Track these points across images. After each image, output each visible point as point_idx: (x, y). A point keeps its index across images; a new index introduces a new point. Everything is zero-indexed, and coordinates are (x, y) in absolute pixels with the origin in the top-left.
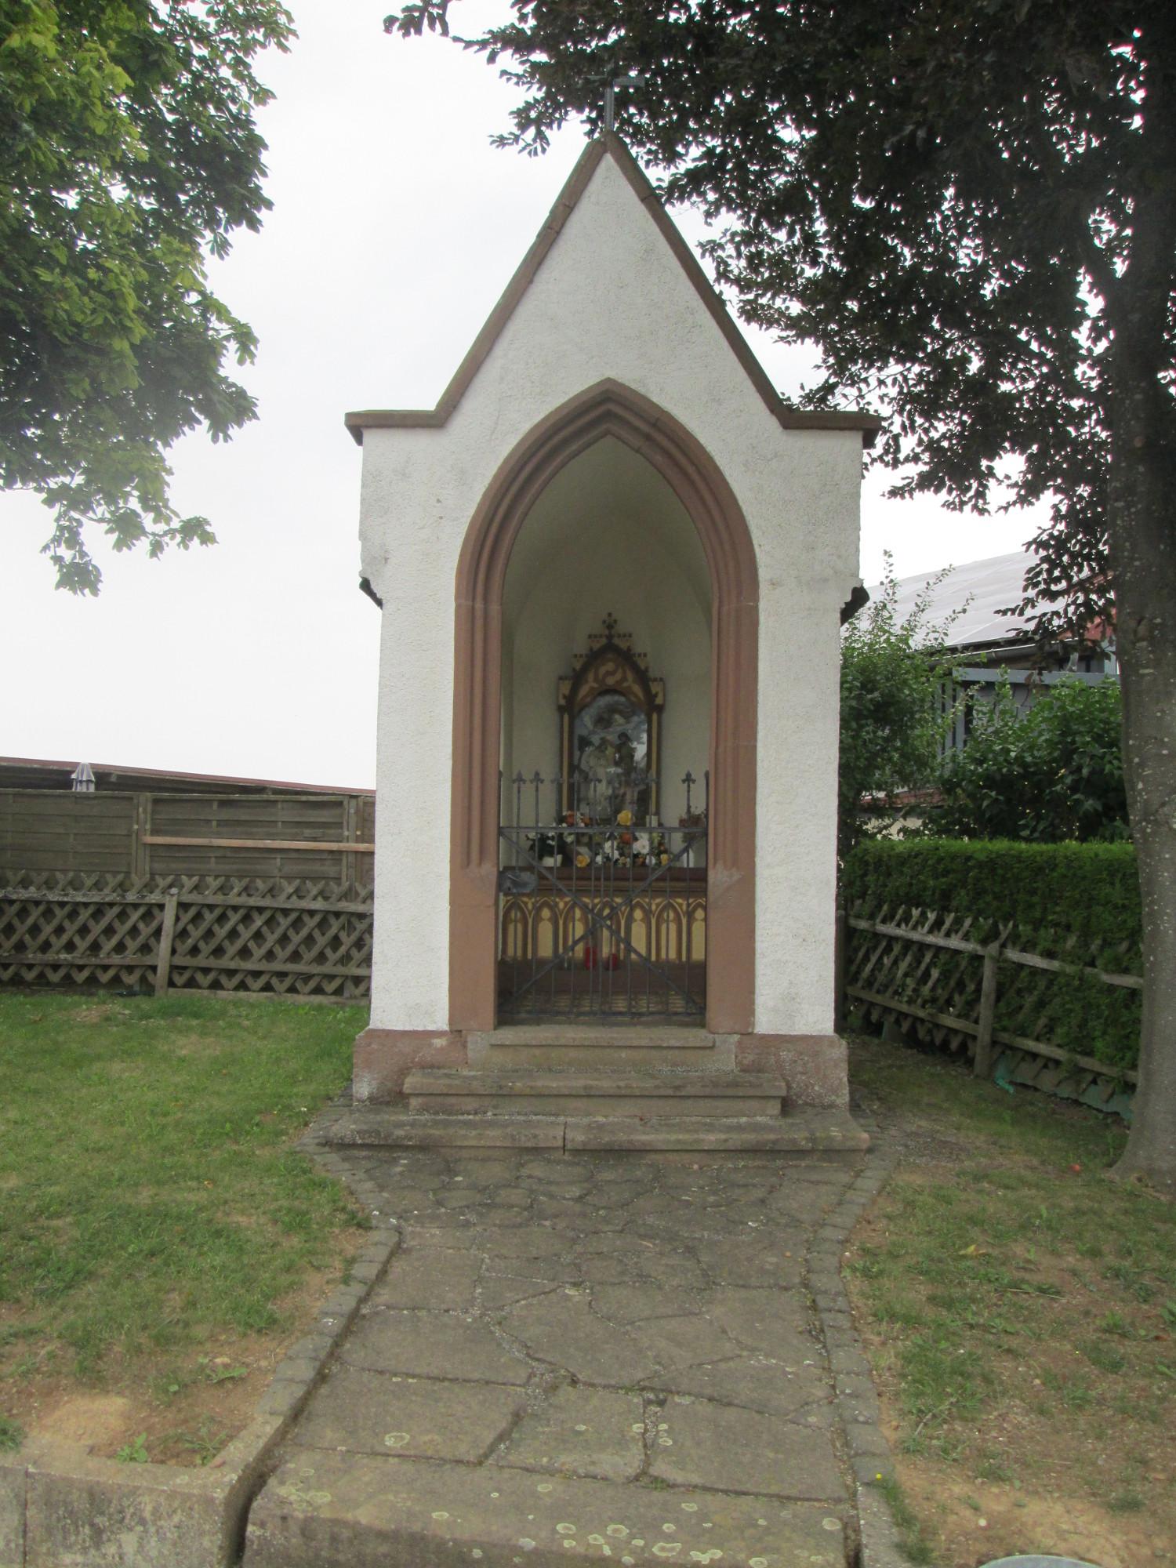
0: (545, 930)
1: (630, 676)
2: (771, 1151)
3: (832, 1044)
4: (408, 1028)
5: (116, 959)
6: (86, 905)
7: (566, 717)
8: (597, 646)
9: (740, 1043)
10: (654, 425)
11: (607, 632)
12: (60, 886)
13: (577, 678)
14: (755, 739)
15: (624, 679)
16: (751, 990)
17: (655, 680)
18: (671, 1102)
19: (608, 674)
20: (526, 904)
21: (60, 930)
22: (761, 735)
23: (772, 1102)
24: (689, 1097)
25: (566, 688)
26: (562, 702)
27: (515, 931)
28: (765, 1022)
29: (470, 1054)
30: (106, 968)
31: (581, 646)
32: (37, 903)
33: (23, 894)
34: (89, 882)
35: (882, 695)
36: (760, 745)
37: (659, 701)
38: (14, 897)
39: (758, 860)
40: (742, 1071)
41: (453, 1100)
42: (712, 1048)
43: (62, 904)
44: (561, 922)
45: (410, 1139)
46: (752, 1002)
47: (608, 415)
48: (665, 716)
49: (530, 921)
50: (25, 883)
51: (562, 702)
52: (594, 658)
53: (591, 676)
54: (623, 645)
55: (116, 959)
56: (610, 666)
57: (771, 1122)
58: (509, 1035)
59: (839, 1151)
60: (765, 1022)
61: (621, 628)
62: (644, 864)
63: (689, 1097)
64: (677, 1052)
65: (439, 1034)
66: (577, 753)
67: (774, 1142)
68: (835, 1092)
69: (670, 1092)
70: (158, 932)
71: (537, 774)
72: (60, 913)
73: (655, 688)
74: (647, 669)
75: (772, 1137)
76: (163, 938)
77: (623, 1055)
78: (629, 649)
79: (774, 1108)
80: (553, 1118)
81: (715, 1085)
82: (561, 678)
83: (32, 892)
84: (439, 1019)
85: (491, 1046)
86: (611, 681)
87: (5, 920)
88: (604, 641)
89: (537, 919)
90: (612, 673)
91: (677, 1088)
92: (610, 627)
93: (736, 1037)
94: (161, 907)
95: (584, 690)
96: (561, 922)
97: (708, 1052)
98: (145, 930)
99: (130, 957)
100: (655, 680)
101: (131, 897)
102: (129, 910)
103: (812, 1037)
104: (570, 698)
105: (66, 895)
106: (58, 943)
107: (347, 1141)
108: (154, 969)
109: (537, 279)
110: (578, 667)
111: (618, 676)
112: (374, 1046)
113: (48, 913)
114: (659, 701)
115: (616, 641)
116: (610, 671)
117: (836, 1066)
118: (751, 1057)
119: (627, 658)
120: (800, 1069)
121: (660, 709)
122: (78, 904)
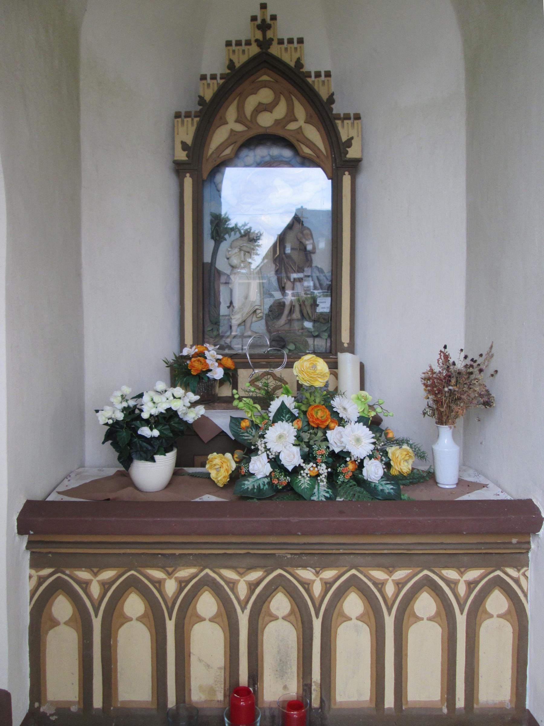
0: (425, 642)
1: (300, 112)
7: (188, 182)
8: (240, 60)
11: (259, 35)
13: (208, 114)
15: (291, 117)
17: (347, 117)
19: (261, 108)
20: (85, 585)
25: (187, 132)
26: (182, 156)
27: (62, 645)
31: (214, 62)
35: (235, 422)
37: (353, 153)
44: (170, 626)
48: (362, 180)
49: (97, 623)
51: (182, 156)
52: (236, 80)
53: (231, 113)
54: (289, 58)
56: (265, 95)
61: (283, 29)
62: (358, 479)
66: (209, 245)
73: (345, 131)
74: (331, 100)
78: (299, 64)
86: (266, 120)
88: (254, 50)
89: (113, 618)
90: (269, 108)
92: (264, 27)
95: (219, 136)
96: (170, 626)
100: (347, 117)
104: (197, 148)
110: (208, 95)
111: (280, 111)
114: (353, 153)
115: (275, 50)
116: (263, 103)
119: (296, 81)
121: (354, 166)
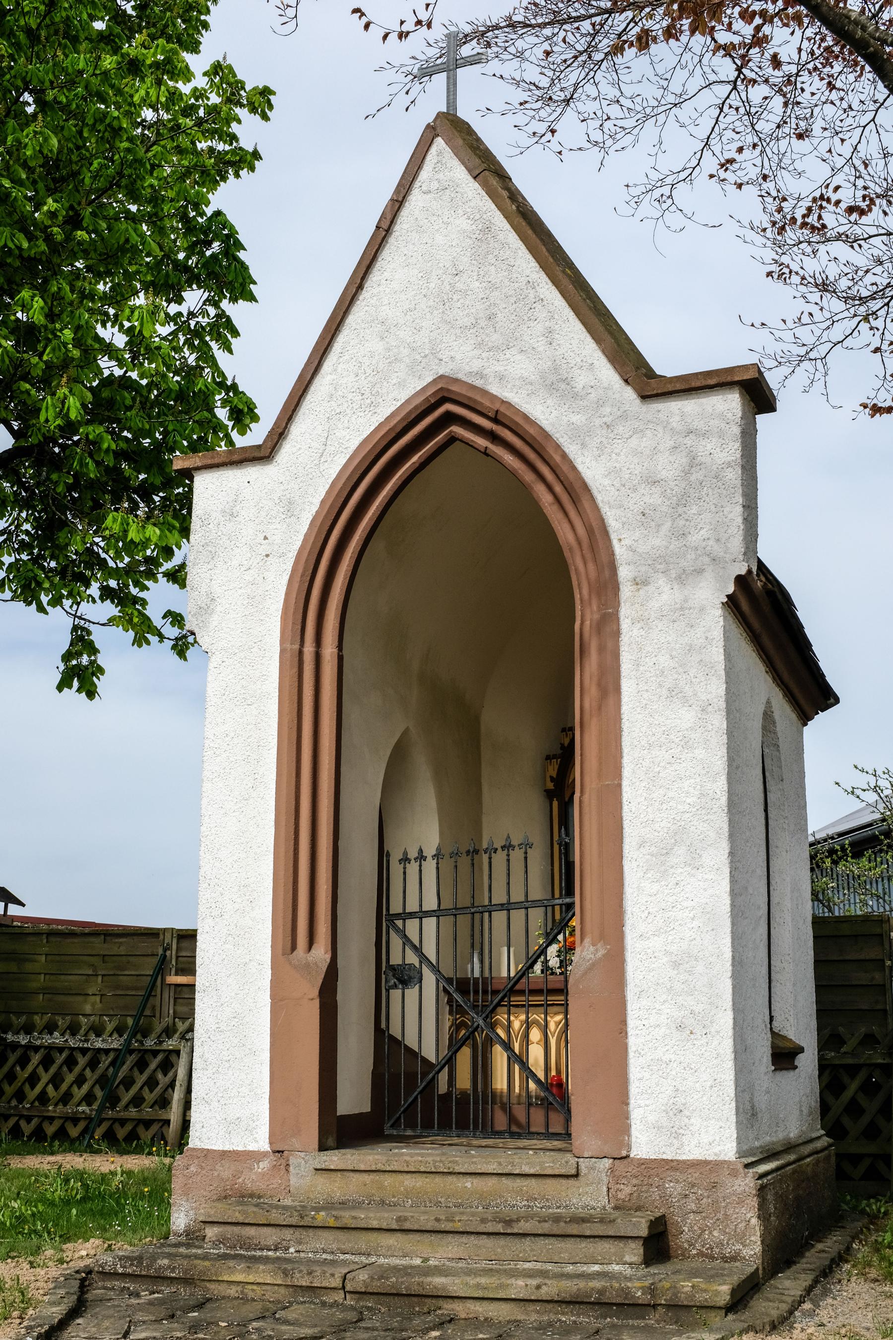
2: (598, 1304)
3: (734, 1174)
4: (227, 1148)
5: (133, 1112)
6: (107, 1051)
9: (612, 1169)
10: (495, 420)
12: (82, 1031)
14: (619, 776)
16: (624, 1099)
18: (502, 1241)
21: (80, 1081)
22: (626, 772)
23: (632, 1245)
24: (525, 1235)
26: (550, 786)
28: (644, 1144)
29: (294, 1181)
30: (123, 1122)
32: (61, 1050)
33: (47, 1040)
34: (110, 1027)
36: (625, 783)
38: (38, 1043)
39: (627, 929)
40: (616, 1208)
41: (251, 1231)
42: (577, 1176)
43: (84, 1051)
45: (173, 1271)
46: (626, 1116)
47: (450, 418)
50: (50, 1028)
51: (550, 786)
55: (133, 1112)
57: (628, 1271)
58: (334, 1159)
59: (688, 1307)
60: (644, 1144)
63: (525, 1235)
64: (533, 1182)
65: (264, 1155)
67: (601, 1292)
68: (741, 1238)
69: (500, 1228)
70: (172, 1085)
71: (421, 851)
72: (82, 1061)
75: (596, 1284)
76: (177, 1088)
77: (469, 1185)
79: (634, 1253)
80: (363, 1258)
81: (557, 1219)
82: (548, 758)
83: (57, 1039)
84: (259, 1139)
85: (311, 1174)
87: (6, 1069)
91: (509, 1223)
93: (607, 1163)
94: (178, 1053)
97: (571, 1182)
98: (163, 1080)
99: (147, 1112)
101: (150, 1043)
102: (148, 1057)
103: (706, 1163)
105: (87, 1041)
106: (79, 1093)
107: (107, 1269)
108: (168, 1122)
109: (368, 284)
112: (193, 1169)
113: (71, 1062)
117: (741, 1202)
118: (627, 1190)
120: (693, 1206)
122: (99, 1050)
